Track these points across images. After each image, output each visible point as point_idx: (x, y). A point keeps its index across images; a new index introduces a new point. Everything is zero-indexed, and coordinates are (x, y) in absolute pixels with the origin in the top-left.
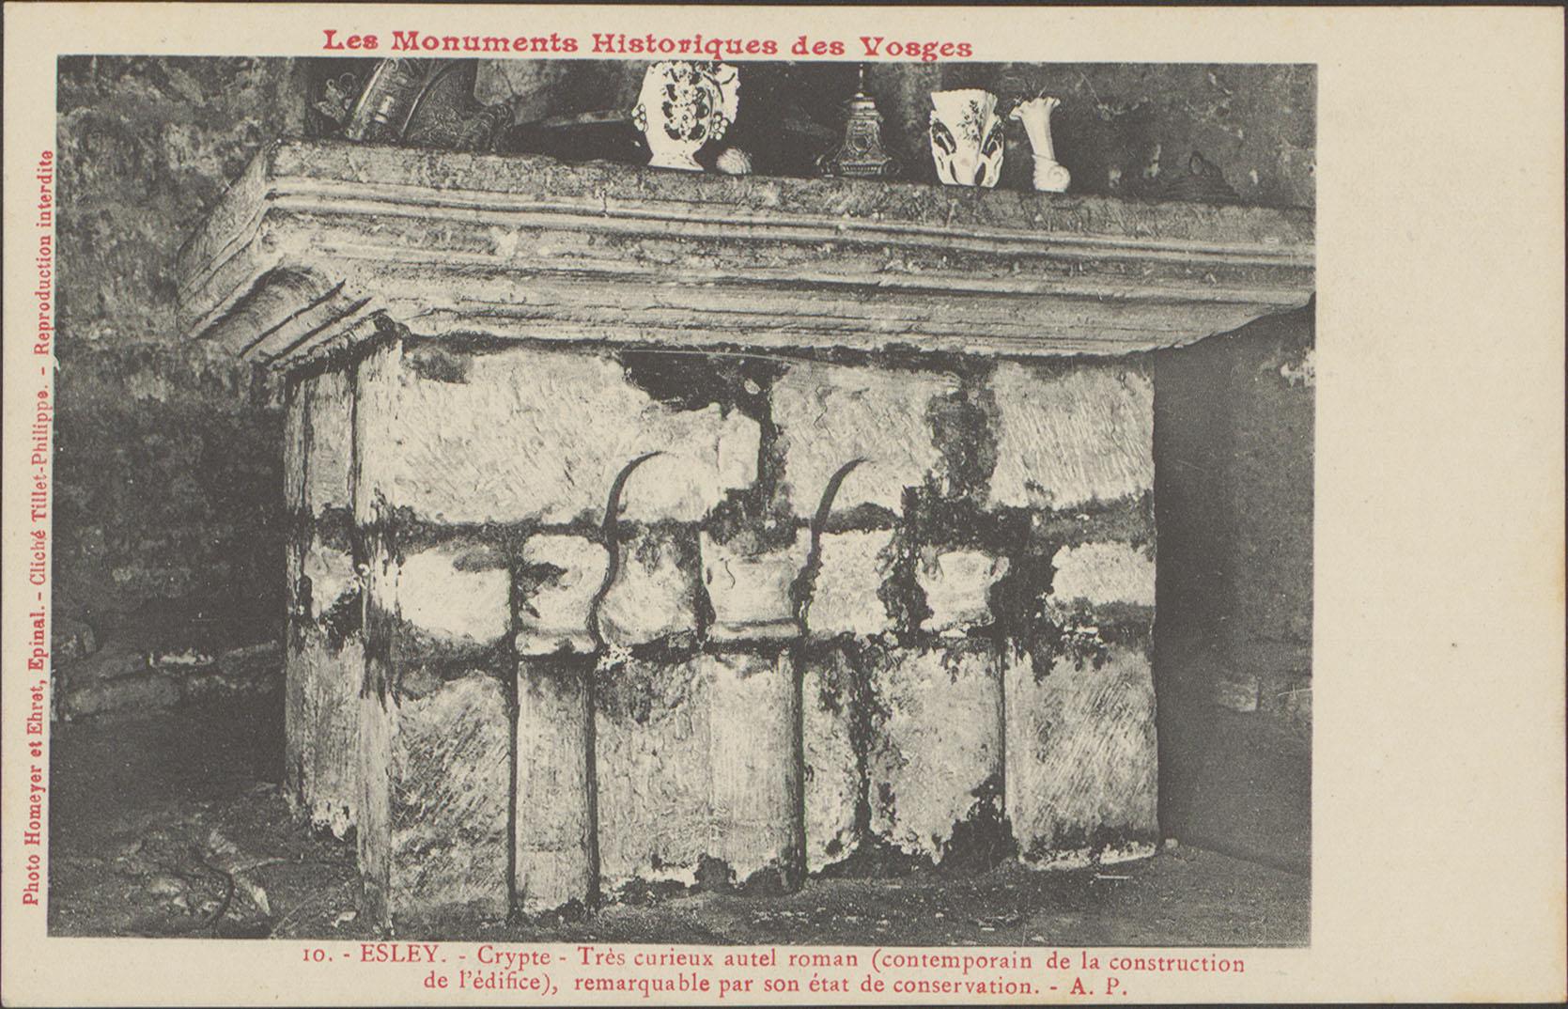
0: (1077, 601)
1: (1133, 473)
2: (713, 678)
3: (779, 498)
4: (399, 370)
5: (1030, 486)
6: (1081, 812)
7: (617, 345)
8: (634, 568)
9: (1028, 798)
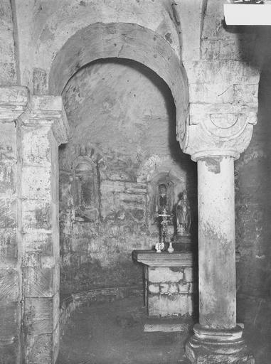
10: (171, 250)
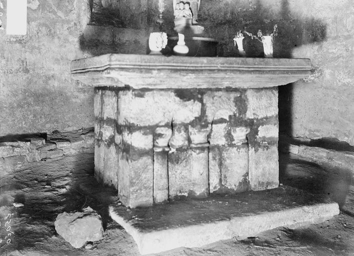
0: (263, 137)
1: (274, 110)
2: (191, 154)
3: (205, 118)
4: (131, 96)
5: (254, 114)
6: (264, 179)
7: (173, 89)
8: (176, 132)
9: (253, 176)
10: (181, 47)
